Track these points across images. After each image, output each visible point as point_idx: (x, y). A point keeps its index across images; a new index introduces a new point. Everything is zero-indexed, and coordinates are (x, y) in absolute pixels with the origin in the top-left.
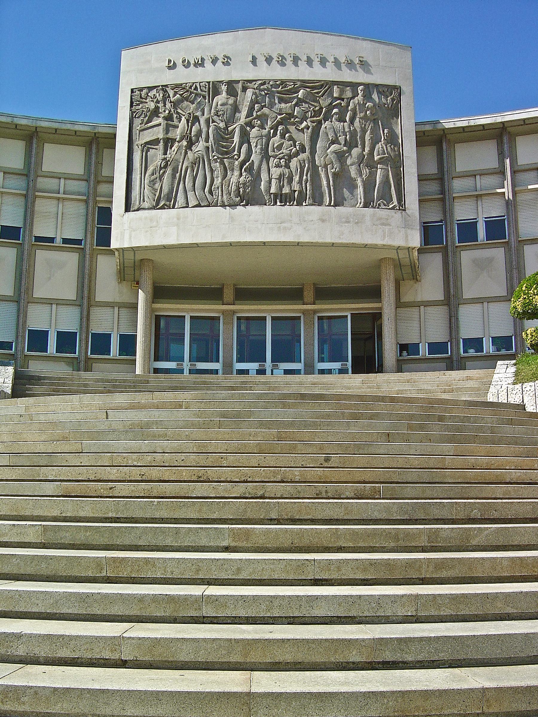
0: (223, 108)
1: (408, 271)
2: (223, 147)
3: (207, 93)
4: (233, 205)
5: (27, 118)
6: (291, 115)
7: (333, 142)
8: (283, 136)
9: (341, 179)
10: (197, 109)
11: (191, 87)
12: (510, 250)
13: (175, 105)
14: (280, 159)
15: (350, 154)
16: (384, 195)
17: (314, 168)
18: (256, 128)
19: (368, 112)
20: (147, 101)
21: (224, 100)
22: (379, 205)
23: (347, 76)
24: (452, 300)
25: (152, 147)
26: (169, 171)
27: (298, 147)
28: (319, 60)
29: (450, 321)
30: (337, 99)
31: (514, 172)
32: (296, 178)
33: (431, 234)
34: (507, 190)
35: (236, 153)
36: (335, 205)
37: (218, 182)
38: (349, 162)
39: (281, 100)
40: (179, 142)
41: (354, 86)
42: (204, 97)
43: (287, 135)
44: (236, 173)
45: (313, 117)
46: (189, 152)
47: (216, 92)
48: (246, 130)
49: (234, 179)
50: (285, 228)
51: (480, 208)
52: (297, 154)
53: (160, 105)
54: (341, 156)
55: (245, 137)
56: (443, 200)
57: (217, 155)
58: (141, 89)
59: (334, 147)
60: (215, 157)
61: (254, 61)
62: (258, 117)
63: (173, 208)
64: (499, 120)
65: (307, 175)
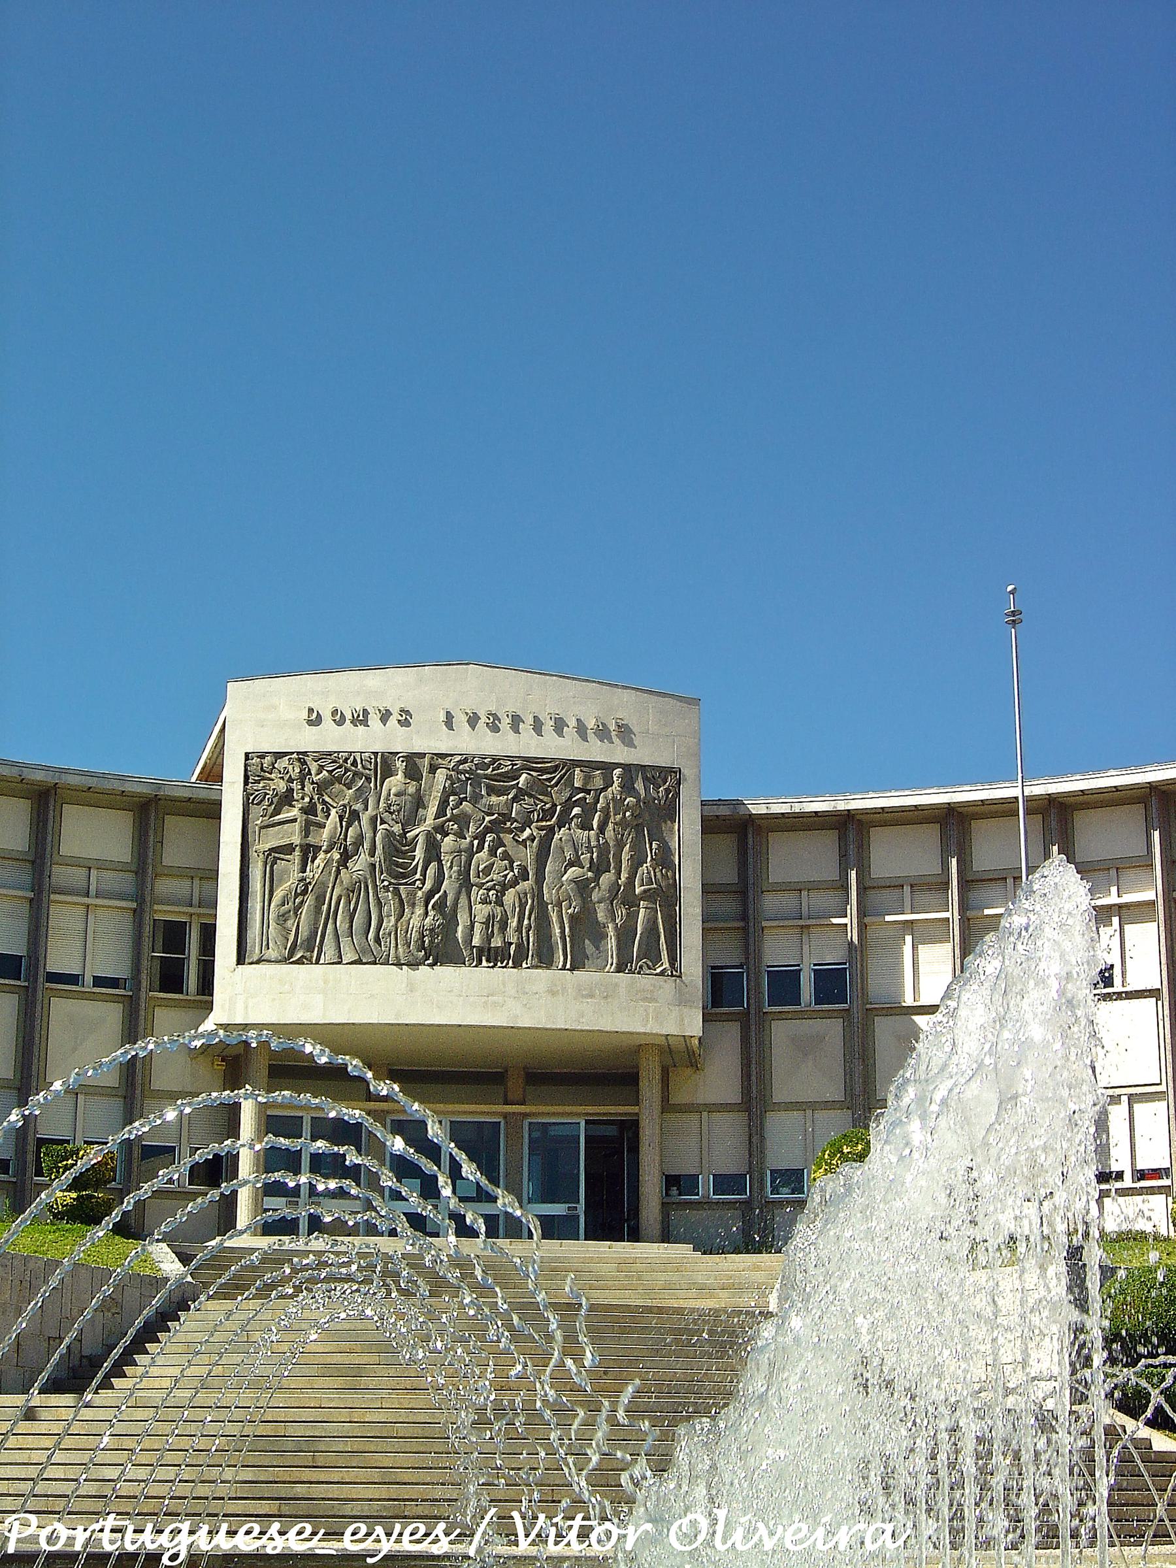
0: (398, 800)
1: (677, 1058)
2: (398, 865)
3: (372, 772)
4: (414, 964)
5: (46, 769)
6: (506, 817)
7: (571, 864)
8: (493, 852)
9: (585, 927)
10: (356, 798)
11: (346, 760)
12: (851, 1024)
13: (321, 787)
14: (489, 890)
15: (598, 884)
16: (646, 952)
17: (541, 906)
18: (451, 837)
19: (628, 814)
20: (273, 776)
21: (401, 787)
22: (641, 967)
23: (596, 751)
24: (754, 1101)
25: (282, 856)
26: (310, 900)
27: (516, 871)
28: (552, 723)
29: (750, 1142)
30: (580, 790)
31: (862, 889)
32: (513, 923)
33: (721, 990)
34: (850, 920)
35: (418, 876)
36: (572, 969)
37: (389, 923)
38: (595, 896)
39: (491, 791)
40: (326, 852)
41: (607, 768)
42: (368, 779)
43: (500, 851)
44: (419, 911)
45: (542, 820)
46: (343, 871)
47: (388, 772)
48: (435, 838)
49: (415, 922)
50: (495, 1004)
51: (806, 948)
52: (515, 883)
53: (295, 786)
54: (583, 887)
55: (433, 852)
56: (745, 930)
57: (389, 879)
58: (262, 756)
59: (573, 872)
60: (386, 883)
61: (449, 721)
62: (453, 819)
63: (317, 963)
64: (842, 806)
65: (529, 919)
